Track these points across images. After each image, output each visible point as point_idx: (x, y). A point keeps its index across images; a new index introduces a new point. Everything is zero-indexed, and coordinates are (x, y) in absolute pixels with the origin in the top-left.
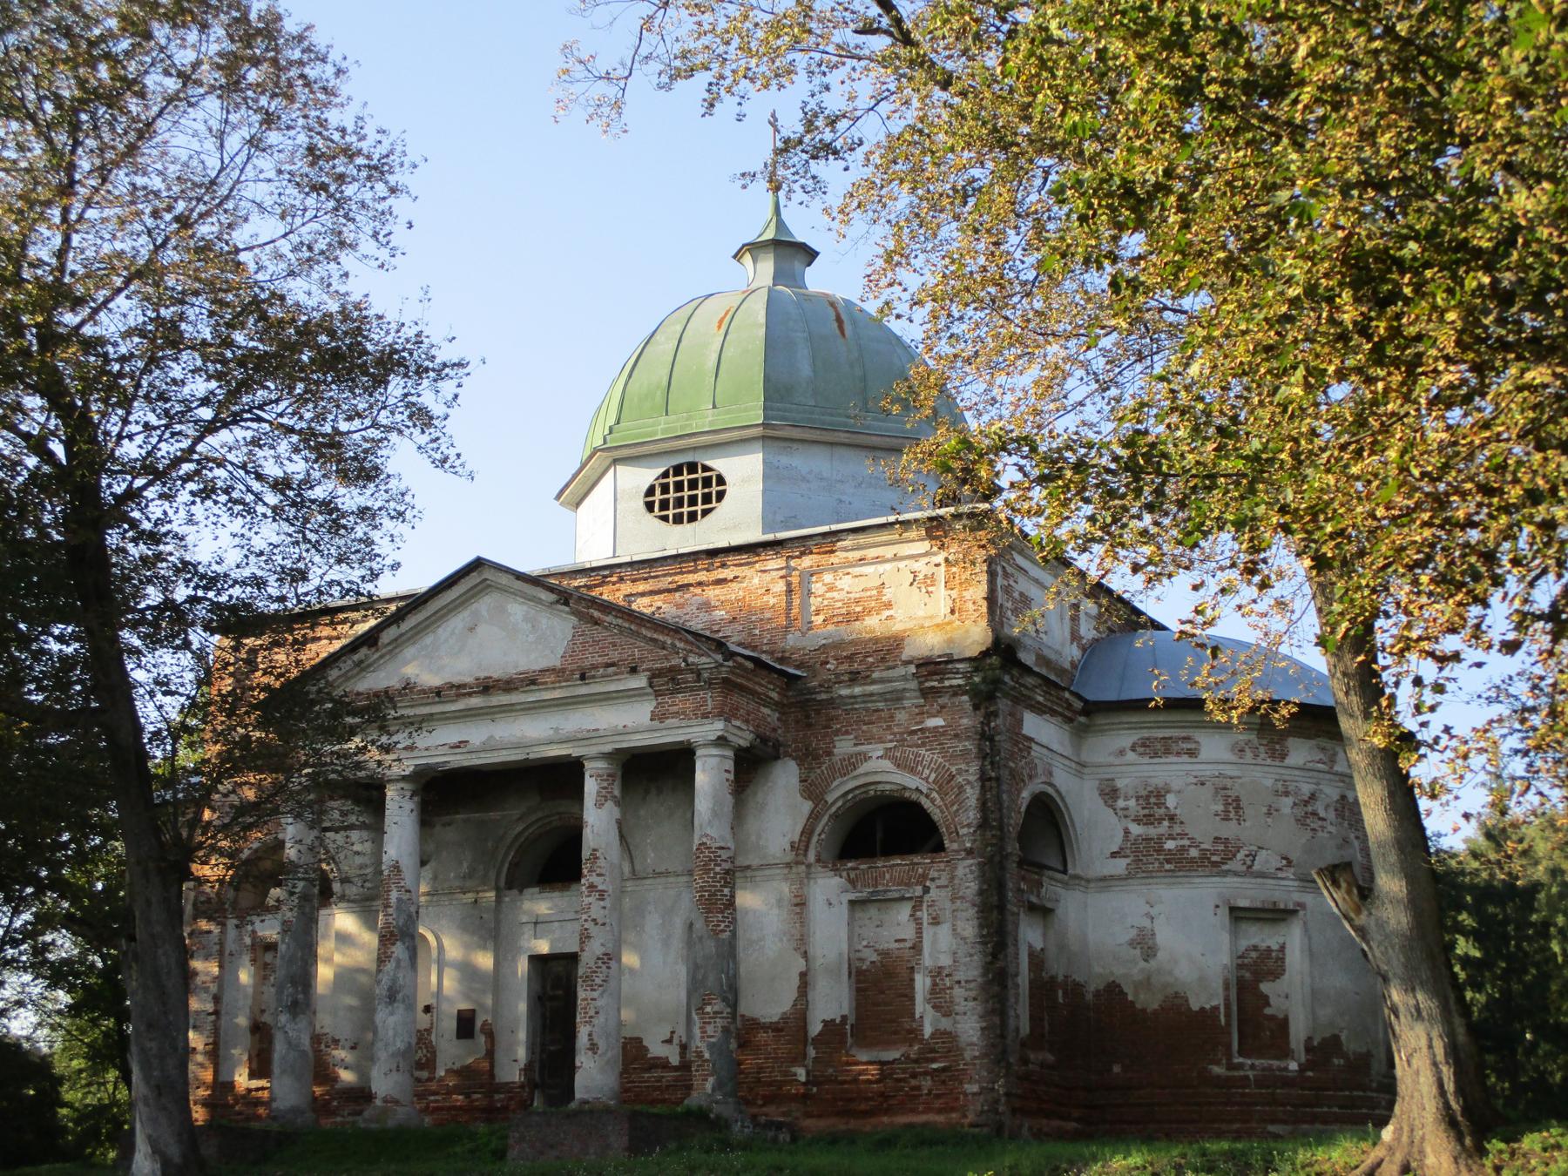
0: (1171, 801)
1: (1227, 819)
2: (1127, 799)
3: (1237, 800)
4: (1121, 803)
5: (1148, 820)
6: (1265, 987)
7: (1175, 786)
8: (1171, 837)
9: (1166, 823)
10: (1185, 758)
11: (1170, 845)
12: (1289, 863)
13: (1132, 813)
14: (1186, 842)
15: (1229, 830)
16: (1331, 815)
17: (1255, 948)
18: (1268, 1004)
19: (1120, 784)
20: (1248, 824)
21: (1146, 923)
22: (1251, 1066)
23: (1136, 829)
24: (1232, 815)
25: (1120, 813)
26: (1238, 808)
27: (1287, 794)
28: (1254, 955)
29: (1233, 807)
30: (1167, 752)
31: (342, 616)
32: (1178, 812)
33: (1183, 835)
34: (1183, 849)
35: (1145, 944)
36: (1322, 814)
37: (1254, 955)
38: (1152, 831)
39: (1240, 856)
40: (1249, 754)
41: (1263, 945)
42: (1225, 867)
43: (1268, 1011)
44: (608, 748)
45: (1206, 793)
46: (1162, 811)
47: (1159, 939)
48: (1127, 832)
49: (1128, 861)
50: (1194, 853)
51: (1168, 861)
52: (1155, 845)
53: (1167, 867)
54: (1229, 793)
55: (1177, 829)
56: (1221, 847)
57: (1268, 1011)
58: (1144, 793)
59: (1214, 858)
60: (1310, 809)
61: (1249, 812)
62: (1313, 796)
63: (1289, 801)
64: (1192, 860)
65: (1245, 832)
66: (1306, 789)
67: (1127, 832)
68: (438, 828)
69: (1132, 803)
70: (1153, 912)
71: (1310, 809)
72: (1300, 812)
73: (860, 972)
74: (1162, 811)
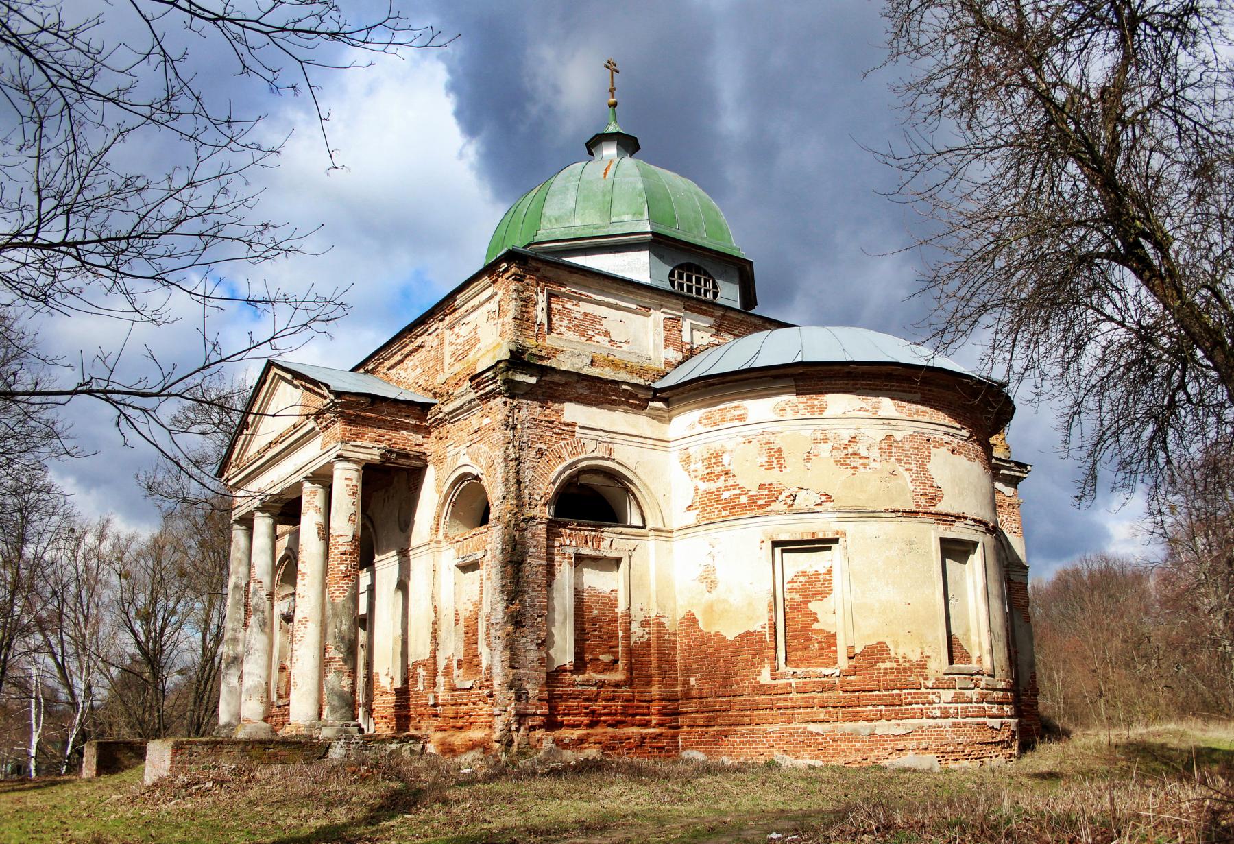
0: (726, 459)
1: (770, 468)
2: (696, 462)
3: (780, 450)
4: (692, 467)
5: (710, 477)
6: (813, 606)
7: (728, 447)
8: (727, 489)
9: (722, 478)
10: (737, 423)
11: (726, 495)
12: (829, 498)
13: (700, 474)
14: (738, 491)
15: (772, 477)
16: (875, 453)
17: (804, 573)
18: (816, 620)
19: (691, 451)
20: (789, 470)
21: (709, 561)
22: (793, 675)
23: (703, 486)
24: (775, 464)
25: (693, 474)
26: (780, 457)
27: (826, 441)
28: (803, 579)
29: (776, 458)
30: (723, 420)
31: (19, 398)
32: (731, 467)
33: (735, 486)
34: (736, 497)
35: (709, 581)
36: (864, 453)
37: (803, 579)
38: (713, 486)
39: (781, 497)
40: (789, 414)
41: (811, 571)
42: (769, 509)
43: (815, 626)
44: (308, 473)
45: (753, 448)
46: (720, 469)
47: (719, 575)
48: (697, 489)
49: (697, 512)
50: (744, 499)
51: (724, 509)
52: (715, 496)
53: (724, 513)
54: (772, 446)
55: (731, 482)
56: (766, 492)
57: (815, 626)
58: (708, 456)
59: (760, 502)
60: (850, 450)
61: (789, 459)
62: (853, 440)
63: (829, 446)
64: (743, 506)
65: (785, 479)
66: (846, 436)
67: (697, 489)
68: (351, 499)
69: (699, 465)
70: (714, 552)
71: (850, 450)
72: (839, 454)
73: (281, 514)
74: (720, 469)
